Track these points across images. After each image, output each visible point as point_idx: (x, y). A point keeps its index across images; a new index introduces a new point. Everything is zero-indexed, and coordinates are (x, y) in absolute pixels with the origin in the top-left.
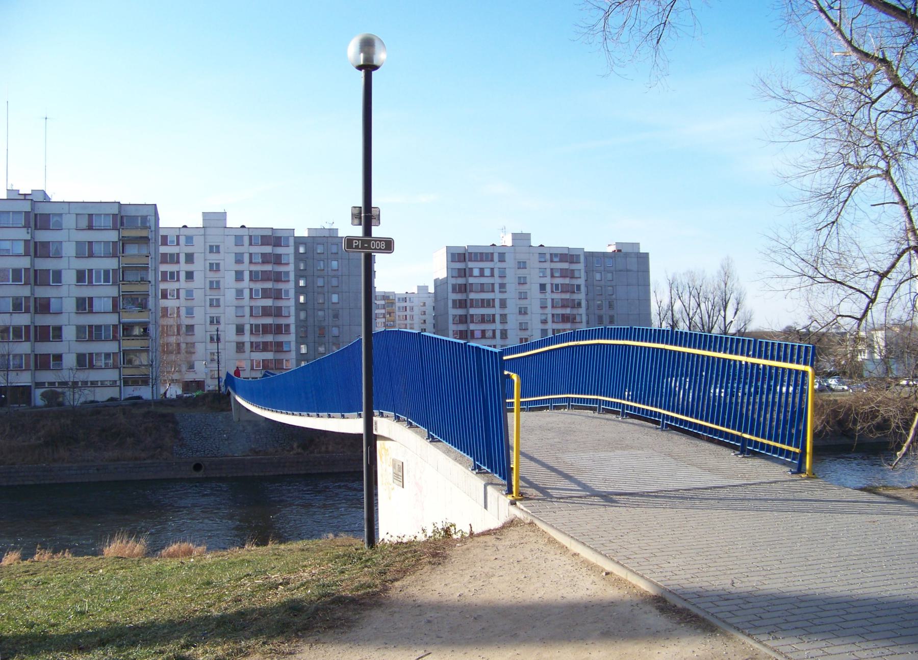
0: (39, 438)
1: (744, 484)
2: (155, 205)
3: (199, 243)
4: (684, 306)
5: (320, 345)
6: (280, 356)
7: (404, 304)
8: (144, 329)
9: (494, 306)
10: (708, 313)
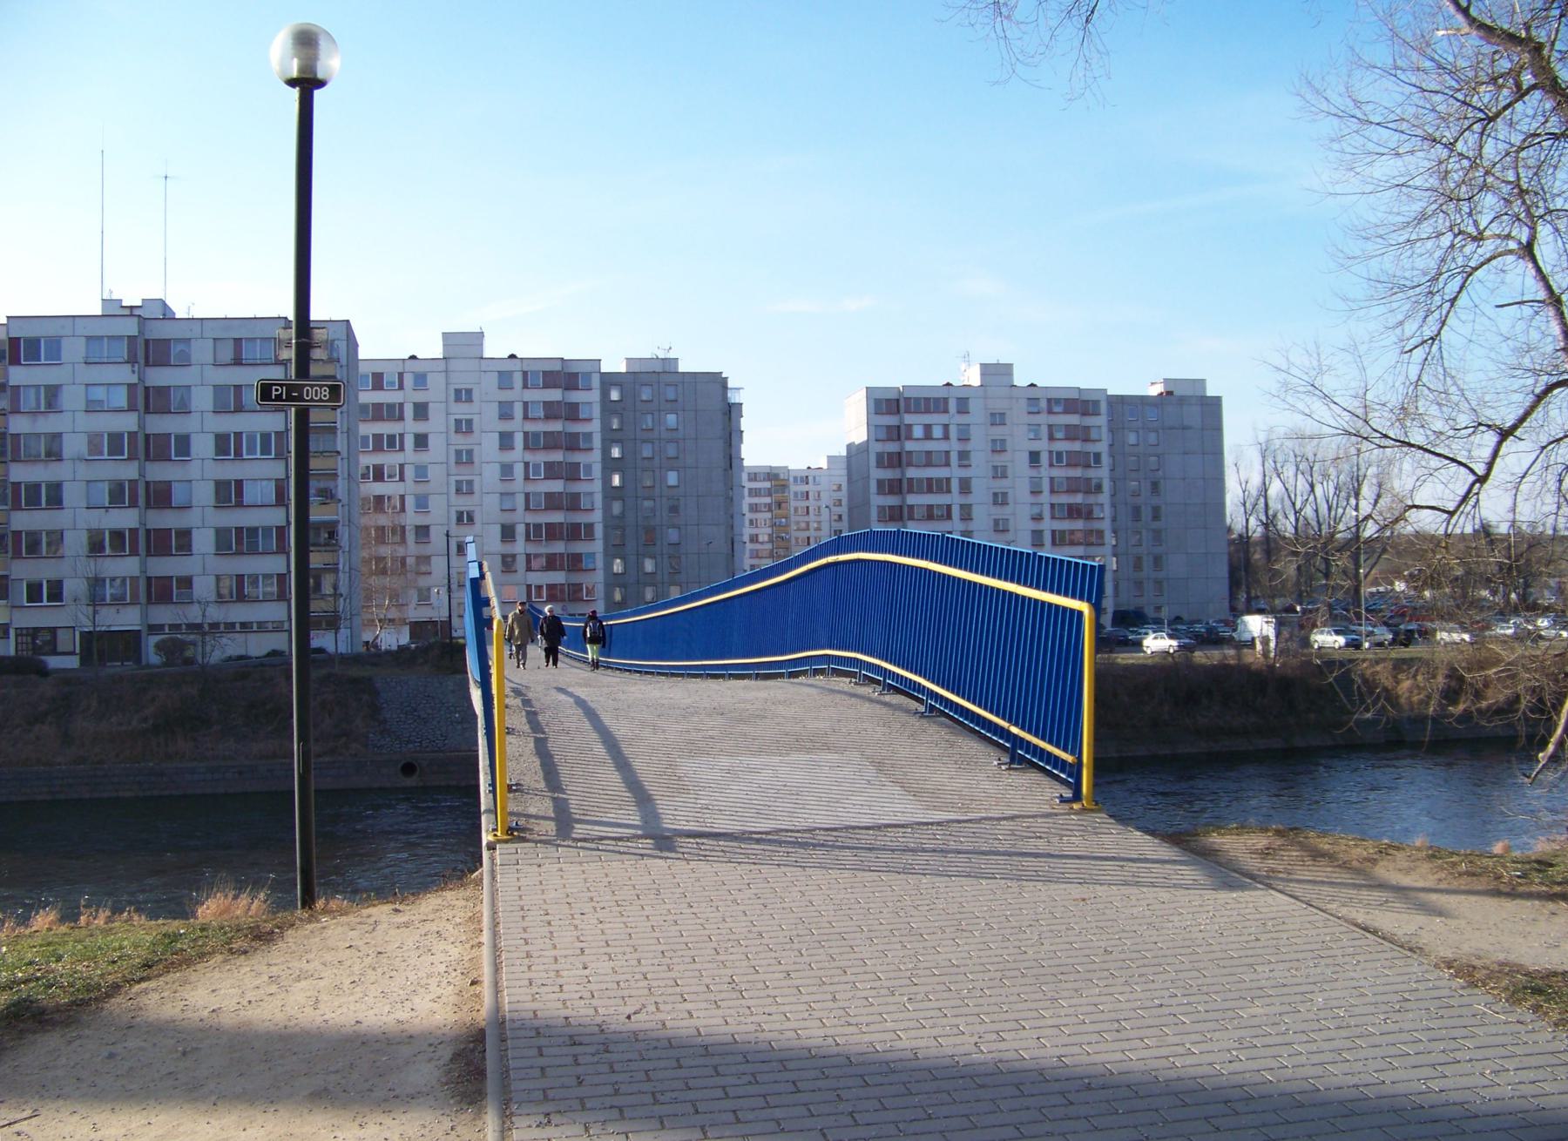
0: (145, 720)
1: (949, 821)
2: (348, 321)
3: (436, 382)
4: (1287, 490)
6: (576, 578)
7: (805, 488)
8: (329, 533)
9: (949, 491)
10: (1328, 502)
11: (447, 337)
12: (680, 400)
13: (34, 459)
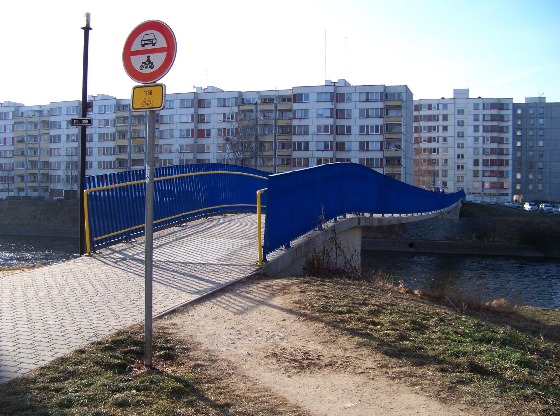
3: (451, 107)
5: (529, 173)
6: (501, 180)
11: (455, 90)
12: (545, 113)
13: (300, 134)
